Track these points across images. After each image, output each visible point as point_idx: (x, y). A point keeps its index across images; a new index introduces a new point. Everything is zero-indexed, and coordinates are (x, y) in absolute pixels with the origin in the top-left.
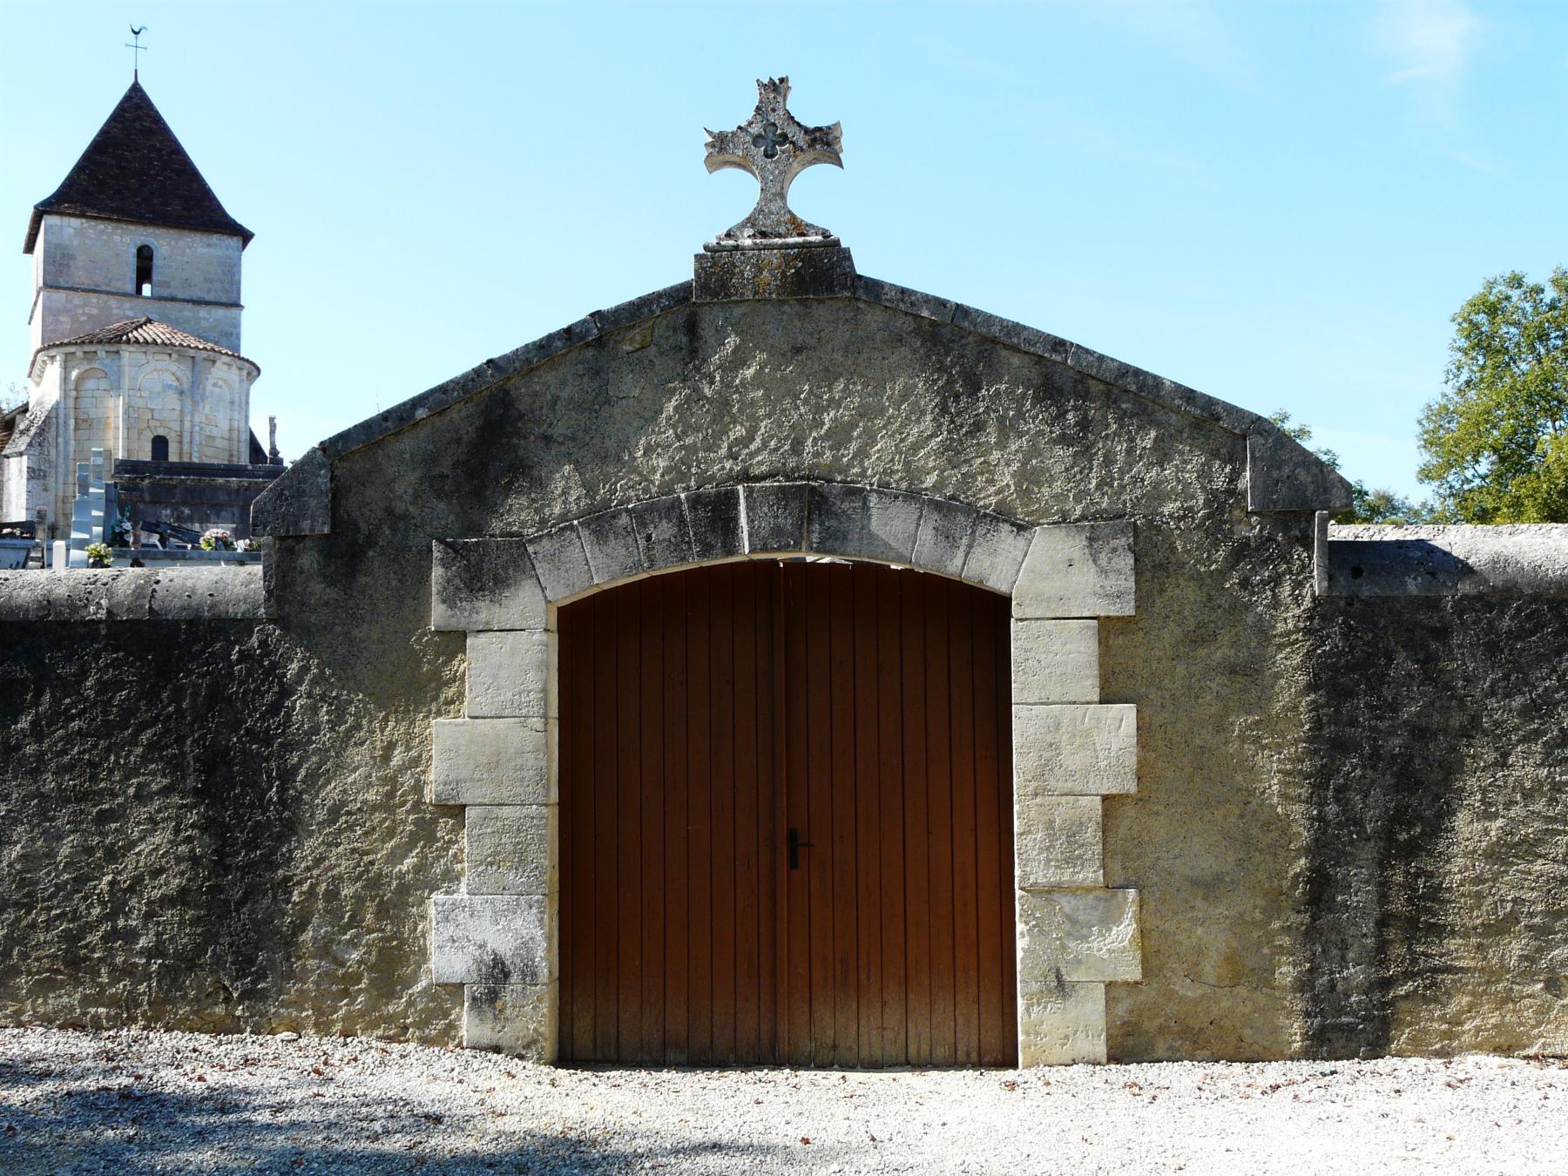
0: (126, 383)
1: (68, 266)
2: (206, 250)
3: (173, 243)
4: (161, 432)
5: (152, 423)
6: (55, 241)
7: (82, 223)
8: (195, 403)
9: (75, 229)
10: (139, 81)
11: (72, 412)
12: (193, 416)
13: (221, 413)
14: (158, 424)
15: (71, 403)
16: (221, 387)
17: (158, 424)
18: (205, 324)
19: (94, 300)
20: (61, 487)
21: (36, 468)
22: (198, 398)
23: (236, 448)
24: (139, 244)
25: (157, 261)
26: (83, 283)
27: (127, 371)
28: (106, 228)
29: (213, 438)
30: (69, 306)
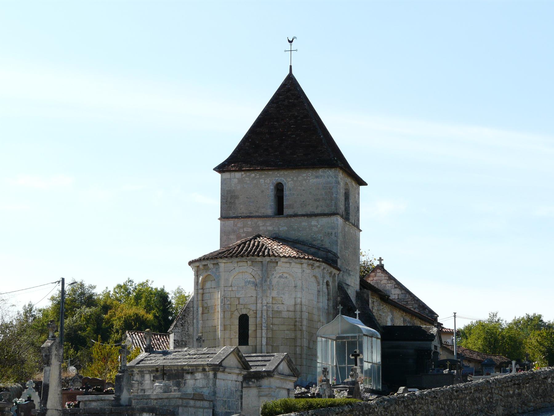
0: (222, 283)
3: (295, 179)
4: (244, 312)
6: (227, 189)
7: (242, 175)
8: (264, 291)
10: (293, 73)
11: (200, 303)
18: (315, 229)
19: (249, 223)
21: (179, 339)
24: (279, 181)
25: (286, 192)
26: (243, 213)
27: (223, 275)
28: (256, 175)
29: (280, 312)
30: (235, 228)
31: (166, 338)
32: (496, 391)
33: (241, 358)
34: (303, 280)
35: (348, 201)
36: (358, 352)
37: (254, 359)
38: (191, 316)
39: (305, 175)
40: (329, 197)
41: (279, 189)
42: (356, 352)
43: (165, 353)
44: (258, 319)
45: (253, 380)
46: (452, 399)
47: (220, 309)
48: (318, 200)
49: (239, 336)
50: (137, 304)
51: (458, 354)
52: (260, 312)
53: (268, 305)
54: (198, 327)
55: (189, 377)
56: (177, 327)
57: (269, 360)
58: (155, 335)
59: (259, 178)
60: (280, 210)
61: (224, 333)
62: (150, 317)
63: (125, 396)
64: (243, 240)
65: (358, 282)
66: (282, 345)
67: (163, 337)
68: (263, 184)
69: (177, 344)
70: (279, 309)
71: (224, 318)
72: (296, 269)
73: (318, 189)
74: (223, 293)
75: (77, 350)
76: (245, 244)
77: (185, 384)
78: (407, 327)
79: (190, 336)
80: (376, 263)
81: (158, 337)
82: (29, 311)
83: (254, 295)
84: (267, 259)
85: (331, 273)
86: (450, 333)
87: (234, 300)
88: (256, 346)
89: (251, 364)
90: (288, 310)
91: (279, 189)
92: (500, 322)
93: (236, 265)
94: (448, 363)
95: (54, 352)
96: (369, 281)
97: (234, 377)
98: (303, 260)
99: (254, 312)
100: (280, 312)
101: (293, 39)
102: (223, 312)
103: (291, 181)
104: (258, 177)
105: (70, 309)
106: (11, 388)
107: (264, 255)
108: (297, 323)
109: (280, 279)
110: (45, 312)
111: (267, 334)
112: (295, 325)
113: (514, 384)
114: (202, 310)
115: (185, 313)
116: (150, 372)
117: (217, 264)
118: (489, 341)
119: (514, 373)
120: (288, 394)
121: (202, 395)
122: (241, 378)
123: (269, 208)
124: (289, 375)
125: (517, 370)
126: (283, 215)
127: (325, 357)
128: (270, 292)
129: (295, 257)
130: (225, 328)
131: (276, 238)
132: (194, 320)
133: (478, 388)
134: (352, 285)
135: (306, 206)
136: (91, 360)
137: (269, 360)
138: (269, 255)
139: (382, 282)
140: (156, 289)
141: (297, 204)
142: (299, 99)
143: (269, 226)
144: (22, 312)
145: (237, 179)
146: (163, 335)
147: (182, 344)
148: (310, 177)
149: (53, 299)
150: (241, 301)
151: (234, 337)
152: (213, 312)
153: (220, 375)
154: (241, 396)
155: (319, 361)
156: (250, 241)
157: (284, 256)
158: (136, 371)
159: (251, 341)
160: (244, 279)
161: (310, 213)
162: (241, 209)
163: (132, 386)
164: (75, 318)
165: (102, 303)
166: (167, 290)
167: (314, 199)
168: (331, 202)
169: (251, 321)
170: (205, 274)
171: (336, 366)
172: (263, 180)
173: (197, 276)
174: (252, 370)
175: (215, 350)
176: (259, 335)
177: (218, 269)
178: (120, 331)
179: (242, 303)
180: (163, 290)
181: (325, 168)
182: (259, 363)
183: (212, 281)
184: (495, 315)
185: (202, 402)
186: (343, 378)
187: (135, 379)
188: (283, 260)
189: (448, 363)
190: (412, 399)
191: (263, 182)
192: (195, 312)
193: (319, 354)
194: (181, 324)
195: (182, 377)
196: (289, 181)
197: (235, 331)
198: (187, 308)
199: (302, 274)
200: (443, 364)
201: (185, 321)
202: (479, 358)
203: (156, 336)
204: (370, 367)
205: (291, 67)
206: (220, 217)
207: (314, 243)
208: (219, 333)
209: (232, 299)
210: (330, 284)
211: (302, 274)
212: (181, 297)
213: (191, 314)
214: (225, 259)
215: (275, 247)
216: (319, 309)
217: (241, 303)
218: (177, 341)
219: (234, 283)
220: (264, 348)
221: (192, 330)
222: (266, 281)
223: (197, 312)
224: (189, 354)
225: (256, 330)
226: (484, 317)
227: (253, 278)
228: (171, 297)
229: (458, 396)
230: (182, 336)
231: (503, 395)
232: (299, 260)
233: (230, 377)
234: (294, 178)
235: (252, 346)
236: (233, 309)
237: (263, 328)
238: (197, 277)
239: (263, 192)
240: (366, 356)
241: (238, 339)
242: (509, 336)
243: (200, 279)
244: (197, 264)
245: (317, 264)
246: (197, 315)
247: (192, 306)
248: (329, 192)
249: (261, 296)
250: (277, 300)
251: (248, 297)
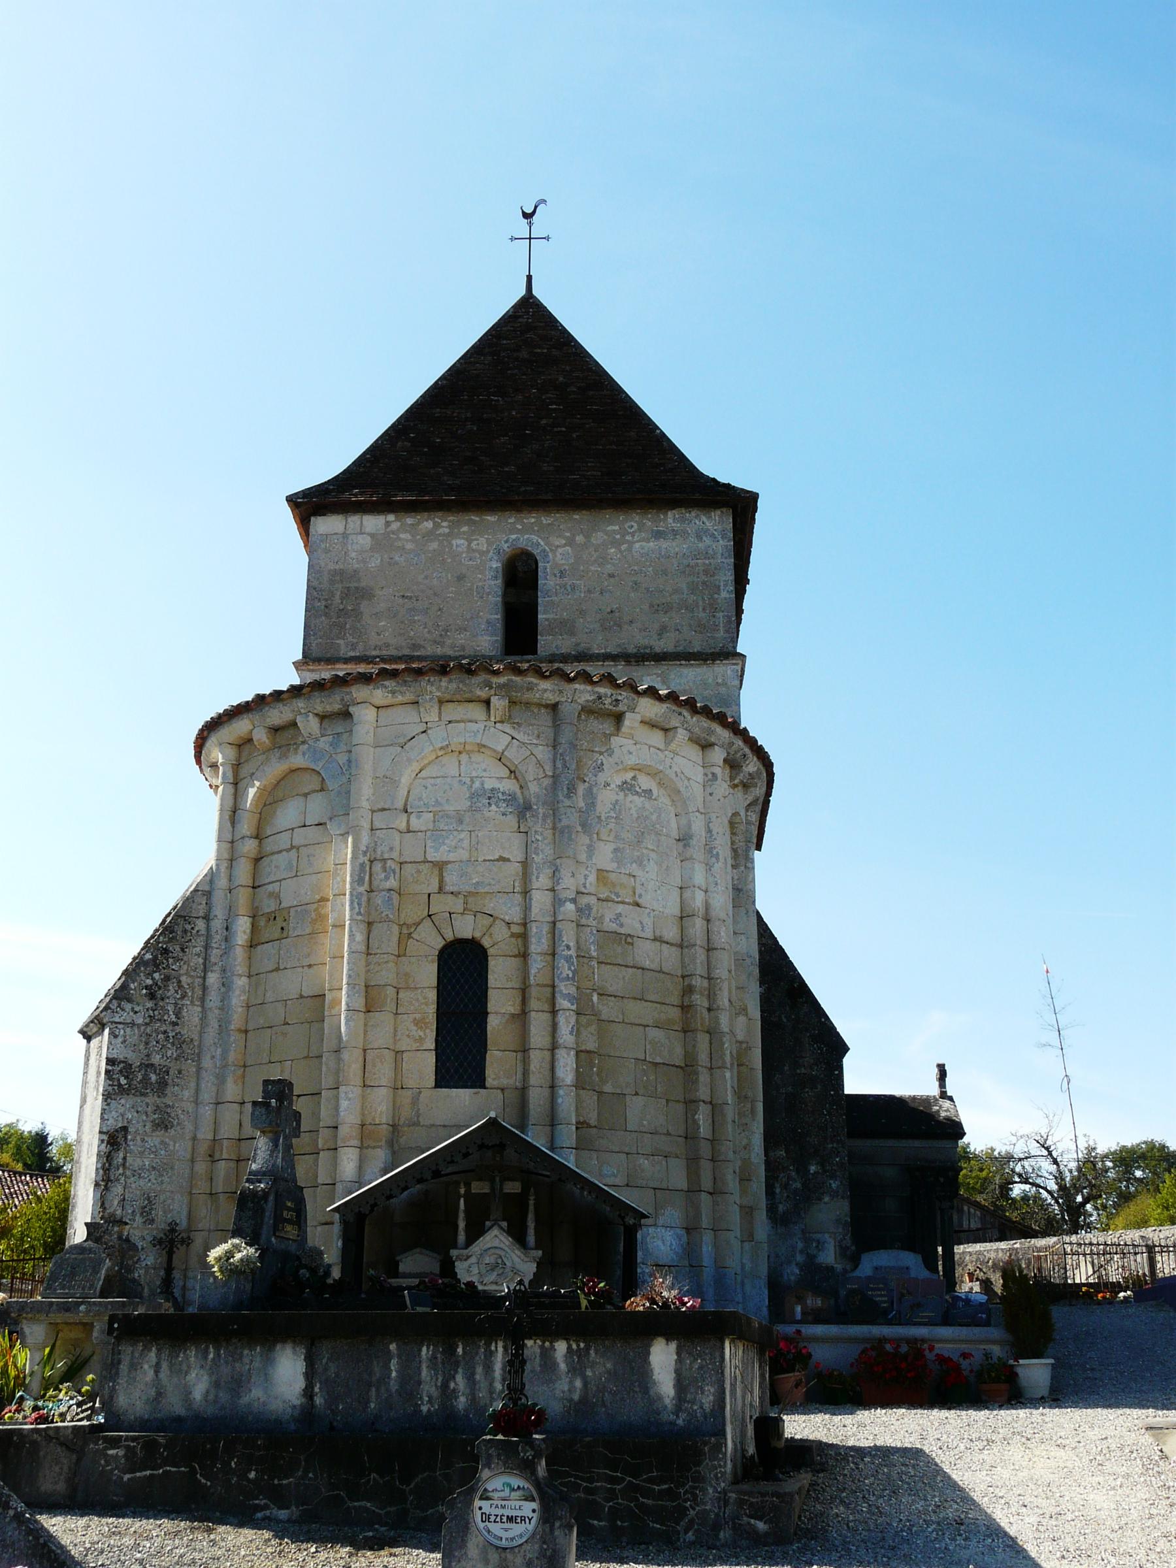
0: (365, 793)
1: (357, 614)
3: (580, 539)
4: (466, 928)
5: (440, 905)
6: (332, 566)
7: (388, 524)
8: (560, 833)
9: (372, 536)
10: (534, 292)
11: (243, 897)
12: (555, 874)
13: (652, 867)
14: (457, 905)
20: (207, 1111)
21: (135, 1059)
22: (570, 819)
23: (700, 970)
25: (547, 582)
26: (388, 645)
27: (369, 761)
28: (437, 526)
29: (627, 939)
31: (43, 1180)
34: (713, 816)
38: (198, 955)
39: (617, 528)
40: (703, 599)
44: (537, 965)
47: (352, 909)
48: (667, 608)
49: (437, 1041)
52: (546, 929)
53: (584, 900)
54: (224, 1007)
56: (129, 1000)
59: (448, 535)
61: (366, 1025)
66: (637, 1094)
67: (37, 1179)
68: (463, 552)
69: (123, 1081)
70: (622, 925)
71: (368, 954)
73: (665, 573)
74: (365, 839)
79: (184, 1046)
81: (25, 1179)
83: (516, 854)
84: (582, 692)
87: (419, 872)
88: (523, 1090)
90: (658, 934)
93: (433, 716)
99: (516, 929)
100: (629, 940)
101: (536, 207)
102: (363, 927)
103: (565, 545)
104: (447, 530)
109: (626, 795)
111: (577, 1031)
114: (248, 931)
115: (171, 940)
117: (346, 715)
126: (536, 653)
128: (588, 841)
132: (210, 974)
135: (620, 626)
141: (589, 620)
142: (565, 348)
145: (368, 534)
146: (36, 1175)
147: (145, 1080)
148: (633, 535)
150: (452, 880)
151: (415, 1046)
152: (308, 931)
160: (468, 781)
161: (635, 651)
162: (378, 634)
167: (651, 606)
168: (714, 616)
170: (276, 768)
172: (462, 541)
176: (538, 1035)
177: (345, 736)
179: (455, 889)
183: (306, 795)
191: (464, 548)
192: (217, 938)
194: (146, 987)
196: (558, 546)
197: (418, 1016)
198: (180, 920)
199: (709, 790)
201: (167, 979)
203: (23, 1178)
205: (529, 278)
209: (408, 868)
211: (709, 790)
213: (198, 949)
214: (387, 683)
217: (448, 888)
218: (122, 1065)
219: (420, 799)
221: (196, 1020)
222: (572, 790)
223: (226, 940)
225: (522, 1017)
227: (509, 778)
230: (147, 1044)
234: (574, 535)
235: (502, 1090)
236: (414, 912)
237: (563, 1003)
238: (232, 791)
239: (461, 578)
241: (431, 1058)
243: (252, 792)
247: (201, 914)
248: (704, 583)
249: (550, 858)
250: (614, 885)
251: (485, 860)
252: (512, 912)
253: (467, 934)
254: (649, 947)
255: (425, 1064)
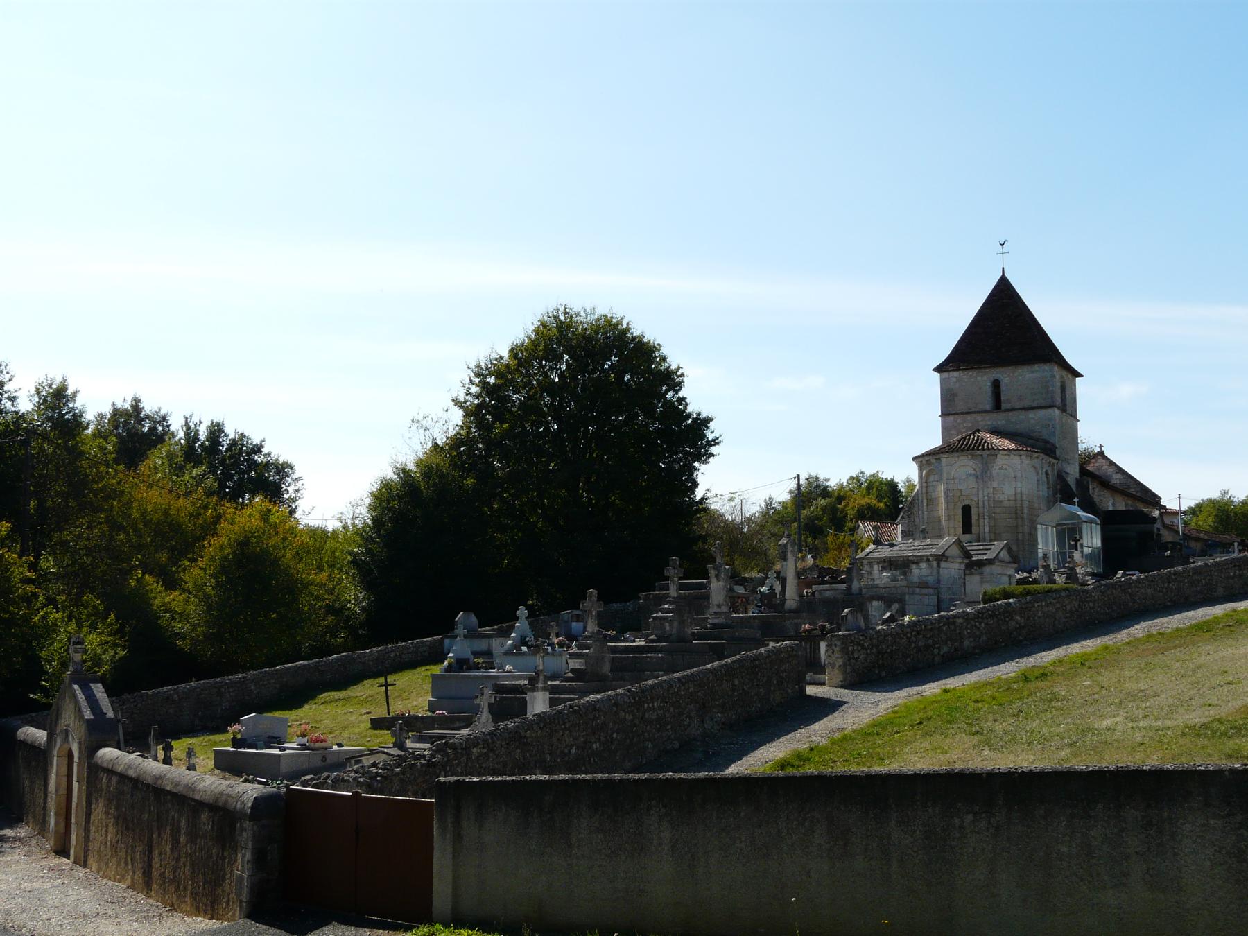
0: (945, 475)
2: (1030, 375)
3: (1011, 375)
14: (965, 498)
15: (924, 490)
16: (1006, 469)
17: (965, 498)
18: (1033, 422)
21: (907, 530)
24: (996, 378)
25: (1003, 388)
29: (1001, 501)
32: (1216, 574)
33: (963, 548)
35: (1065, 391)
36: (1078, 538)
37: (975, 548)
41: (996, 385)
42: (1076, 537)
43: (892, 545)
44: (981, 510)
45: (975, 568)
46: (1169, 583)
50: (869, 494)
51: (1183, 534)
55: (914, 566)
57: (990, 549)
58: (886, 523)
60: (997, 405)
62: (882, 505)
63: (856, 585)
64: (963, 435)
65: (1077, 470)
72: (1015, 460)
75: (814, 538)
76: (965, 439)
77: (911, 573)
78: (1129, 510)
80: (1097, 450)
82: (769, 503)
85: (1050, 462)
86: (1175, 513)
88: (979, 534)
89: (972, 553)
91: (996, 385)
92: (1232, 499)
94: (1170, 545)
95: (790, 548)
96: (1088, 468)
97: (957, 566)
98: (1022, 452)
105: (807, 500)
106: (755, 577)
107: (983, 449)
108: (1018, 512)
110: (784, 504)
111: (989, 523)
112: (1016, 514)
113: (1235, 566)
116: (878, 563)
117: (939, 459)
118: (1221, 518)
119: (1236, 555)
120: (1010, 579)
121: (927, 583)
122: (963, 567)
123: (987, 404)
124: (1009, 562)
125: (1240, 551)
127: (1046, 543)
129: (1013, 449)
130: (949, 518)
131: (995, 432)
133: (1197, 571)
134: (1072, 472)
136: (826, 551)
137: (990, 549)
138: (988, 449)
139: (1103, 468)
140: (886, 479)
143: (988, 420)
144: (763, 504)
149: (791, 492)
153: (943, 564)
154: (964, 583)
155: (1040, 547)
156: (970, 436)
157: (1003, 449)
158: (865, 562)
159: (974, 529)
163: (862, 575)
164: (811, 509)
165: (836, 494)
166: (896, 480)
169: (974, 511)
170: (928, 469)
171: (1057, 551)
173: (921, 470)
174: (974, 559)
175: (937, 542)
176: (981, 524)
178: (854, 520)
180: (892, 480)
181: (1041, 363)
182: (980, 552)
184: (1226, 493)
185: (927, 590)
186: (1064, 564)
187: (865, 569)
188: (1002, 452)
189: (1170, 545)
190: (1129, 583)
193: (1040, 540)
195: (908, 567)
200: (1165, 547)
202: (1206, 537)
204: (1090, 552)
205: (1003, 268)
206: (940, 414)
207: (1032, 435)
208: (944, 523)
210: (1050, 473)
212: (911, 487)
215: (994, 440)
216: (1039, 497)
220: (987, 537)
222: (986, 472)
224: (914, 546)
225: (978, 520)
226: (1215, 495)
228: (902, 487)
229: (1176, 579)
231: (1223, 576)
232: (1017, 452)
233: (952, 565)
237: (986, 517)
239: (980, 388)
240: (1086, 540)
242: (1242, 512)
243: (924, 473)
244: (921, 460)
245: (1036, 455)
246: (923, 506)
252: (976, 499)
253: (967, 504)
254: (1006, 502)
255: (961, 530)
